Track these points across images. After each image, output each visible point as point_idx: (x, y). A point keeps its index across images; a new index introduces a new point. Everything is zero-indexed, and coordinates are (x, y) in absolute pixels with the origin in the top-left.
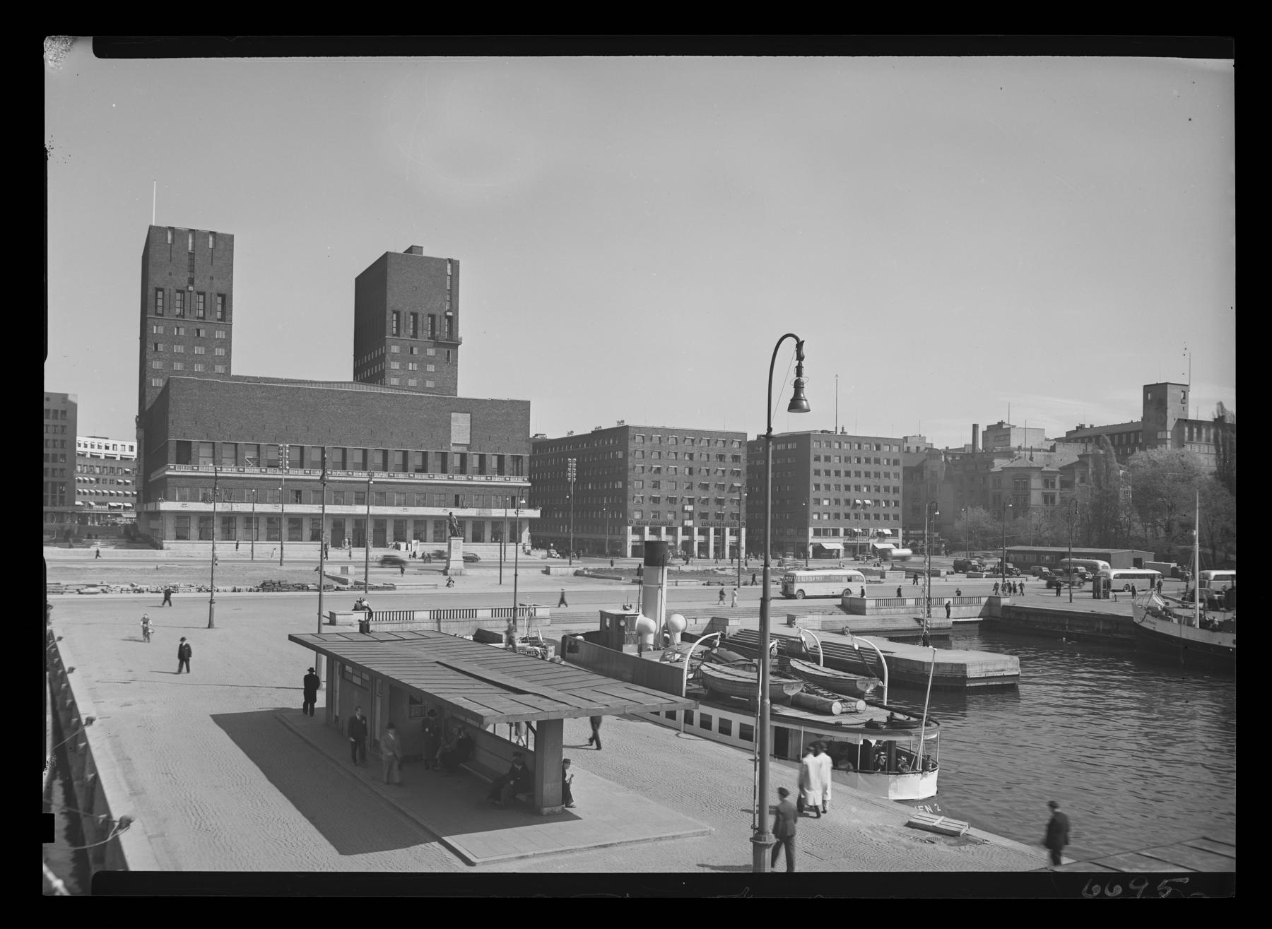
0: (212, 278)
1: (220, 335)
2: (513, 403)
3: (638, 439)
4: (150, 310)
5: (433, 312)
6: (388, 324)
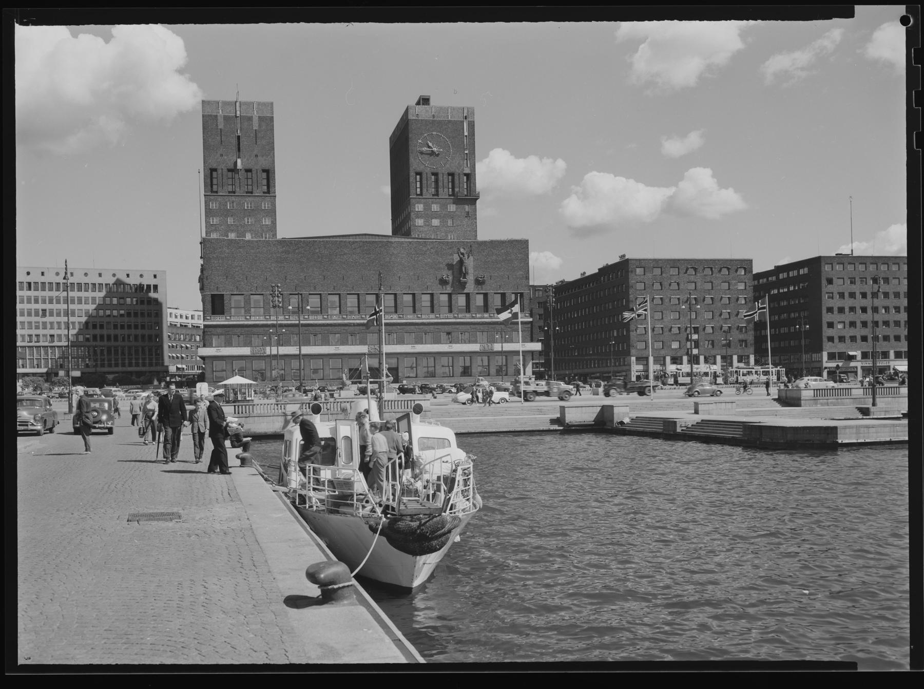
0: (256, 156)
1: (265, 205)
2: (512, 243)
3: (639, 271)
5: (452, 171)
6: (412, 185)
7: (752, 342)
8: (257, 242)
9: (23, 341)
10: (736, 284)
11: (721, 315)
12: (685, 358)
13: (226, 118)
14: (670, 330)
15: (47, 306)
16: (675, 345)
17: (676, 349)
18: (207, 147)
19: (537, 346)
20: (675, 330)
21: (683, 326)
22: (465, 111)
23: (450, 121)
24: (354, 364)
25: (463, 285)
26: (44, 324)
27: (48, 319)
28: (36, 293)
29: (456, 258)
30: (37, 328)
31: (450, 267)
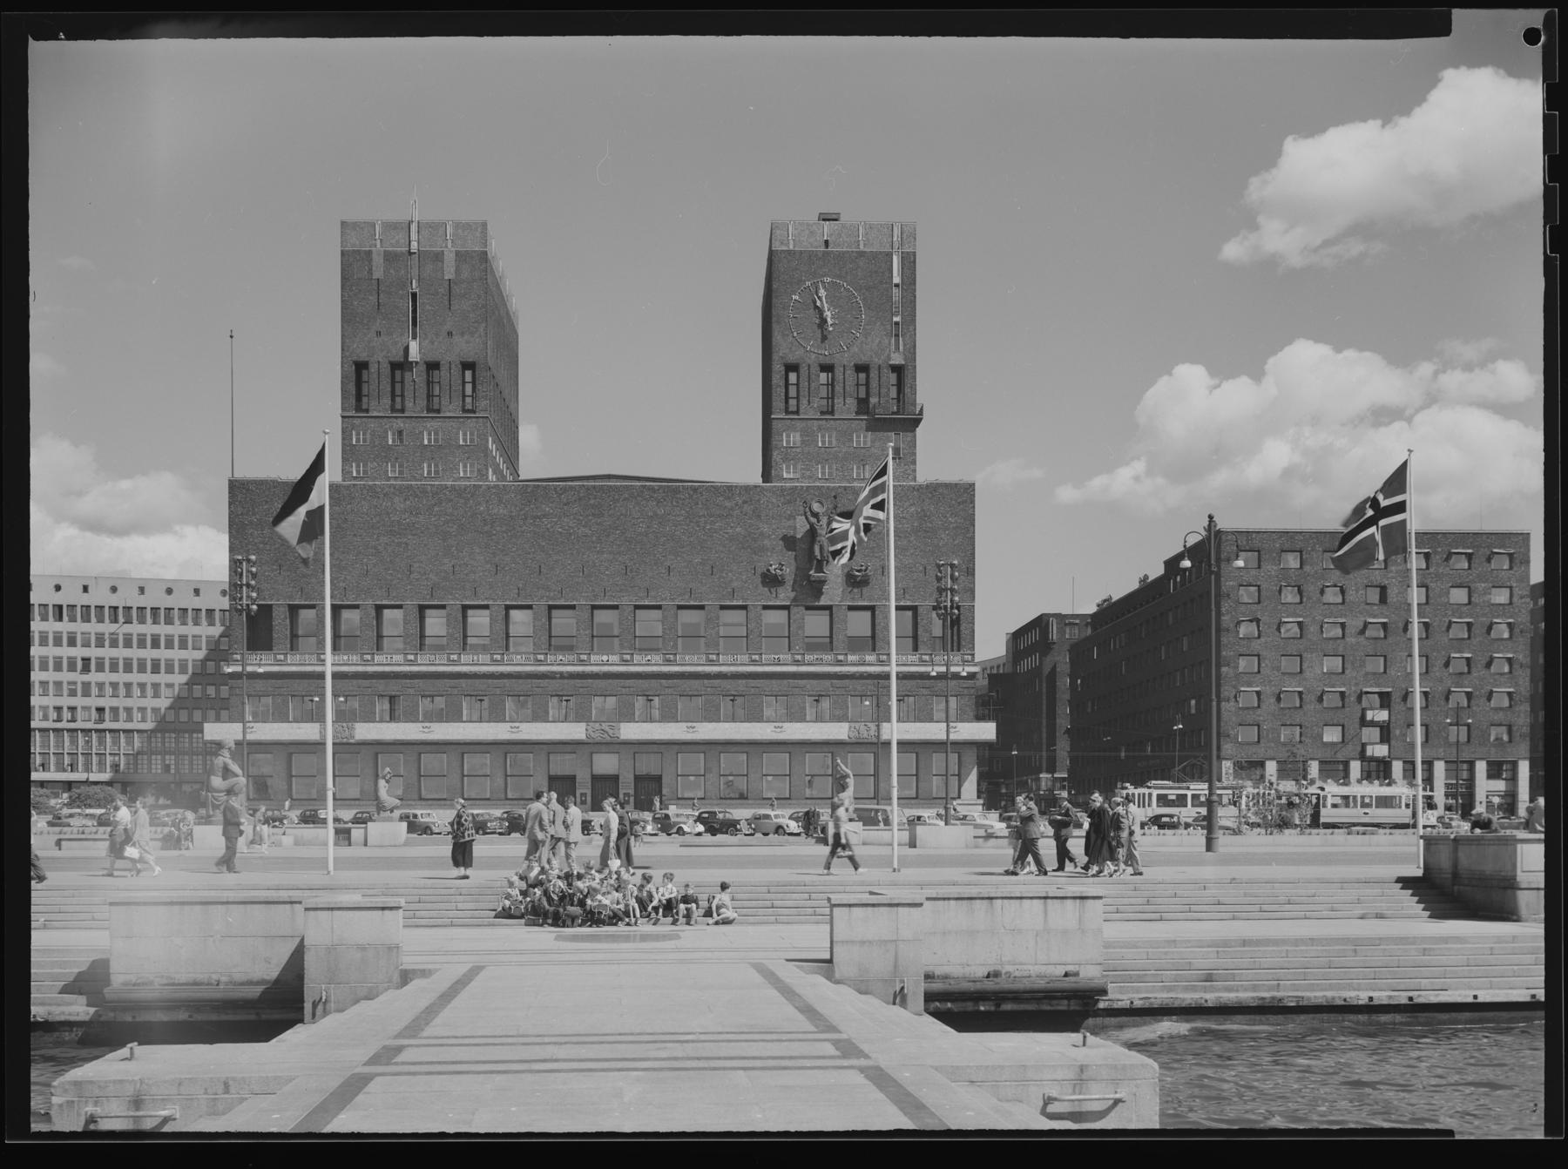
0: (450, 334)
4: (778, 403)
5: (864, 359)
7: (1526, 730)
8: (348, 487)
9: (45, 718)
10: (1487, 592)
11: (1447, 665)
12: (1355, 767)
13: (390, 257)
14: (1320, 699)
15: (93, 652)
16: (1332, 735)
17: (1333, 744)
18: (349, 317)
19: (986, 731)
20: (1331, 701)
21: (1351, 691)
22: (896, 232)
23: (862, 254)
24: (562, 765)
25: (817, 588)
26: (86, 686)
27: (94, 677)
28: (72, 627)
29: (801, 526)
30: (73, 693)
31: (789, 542)
